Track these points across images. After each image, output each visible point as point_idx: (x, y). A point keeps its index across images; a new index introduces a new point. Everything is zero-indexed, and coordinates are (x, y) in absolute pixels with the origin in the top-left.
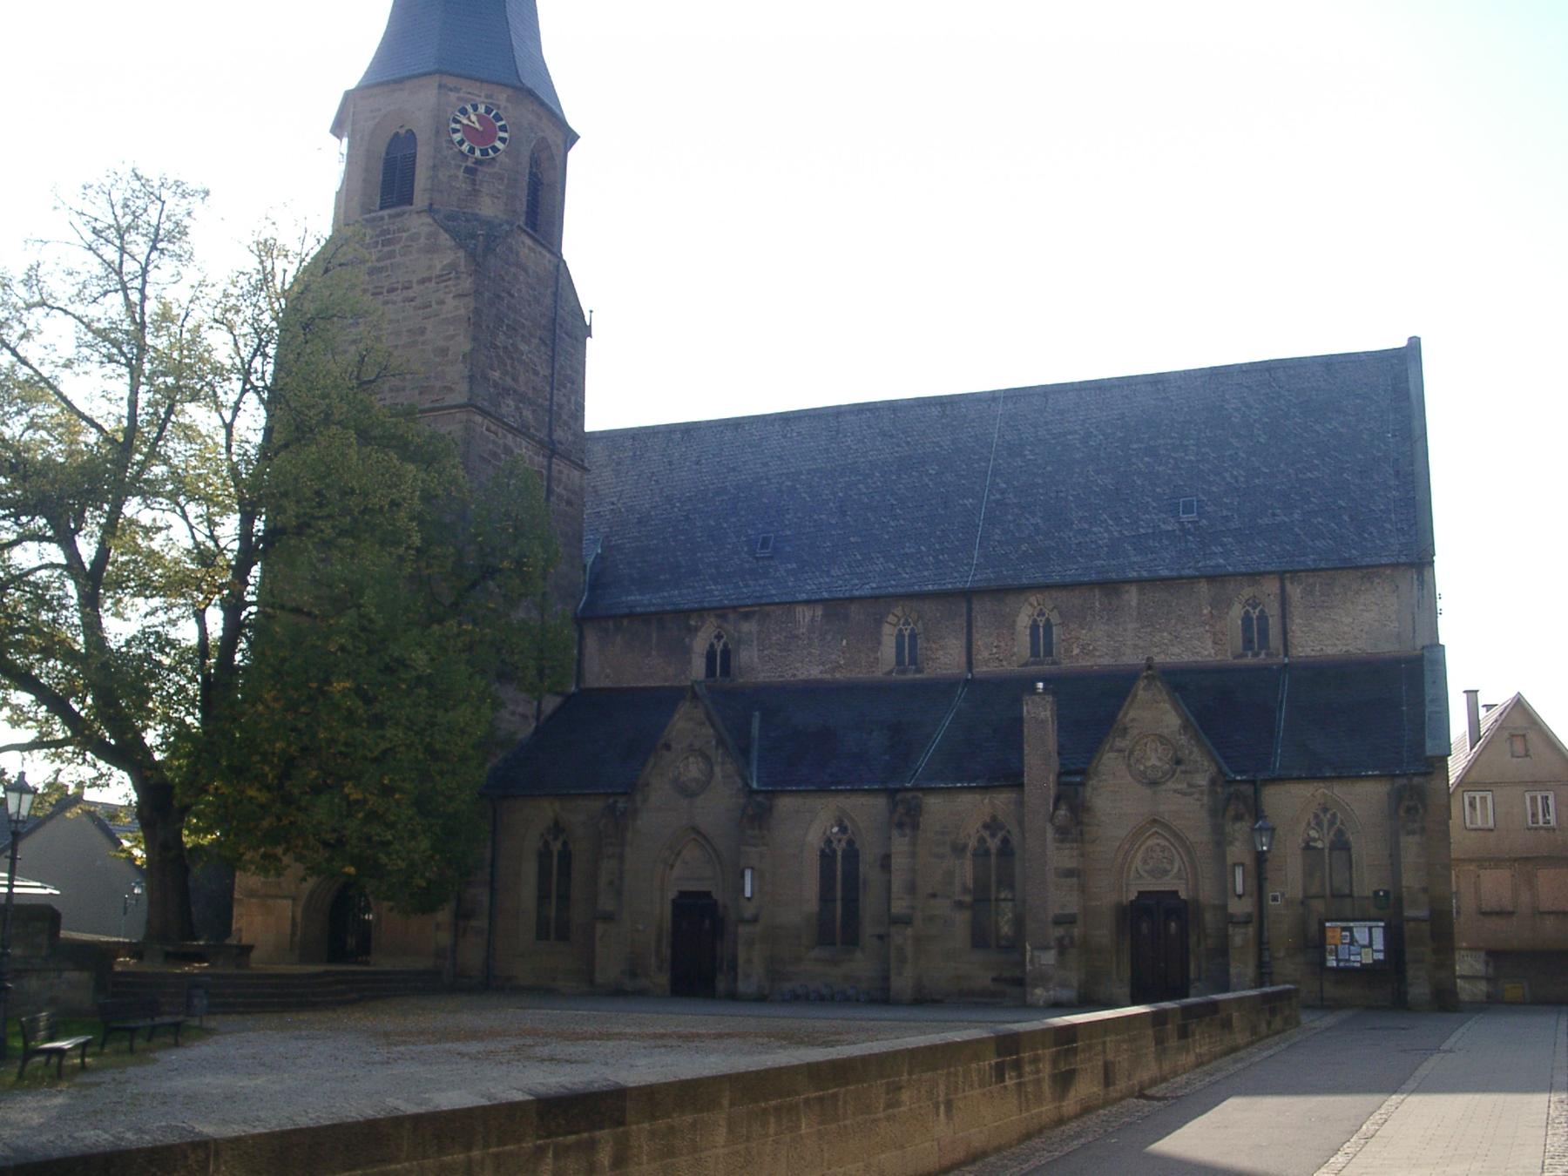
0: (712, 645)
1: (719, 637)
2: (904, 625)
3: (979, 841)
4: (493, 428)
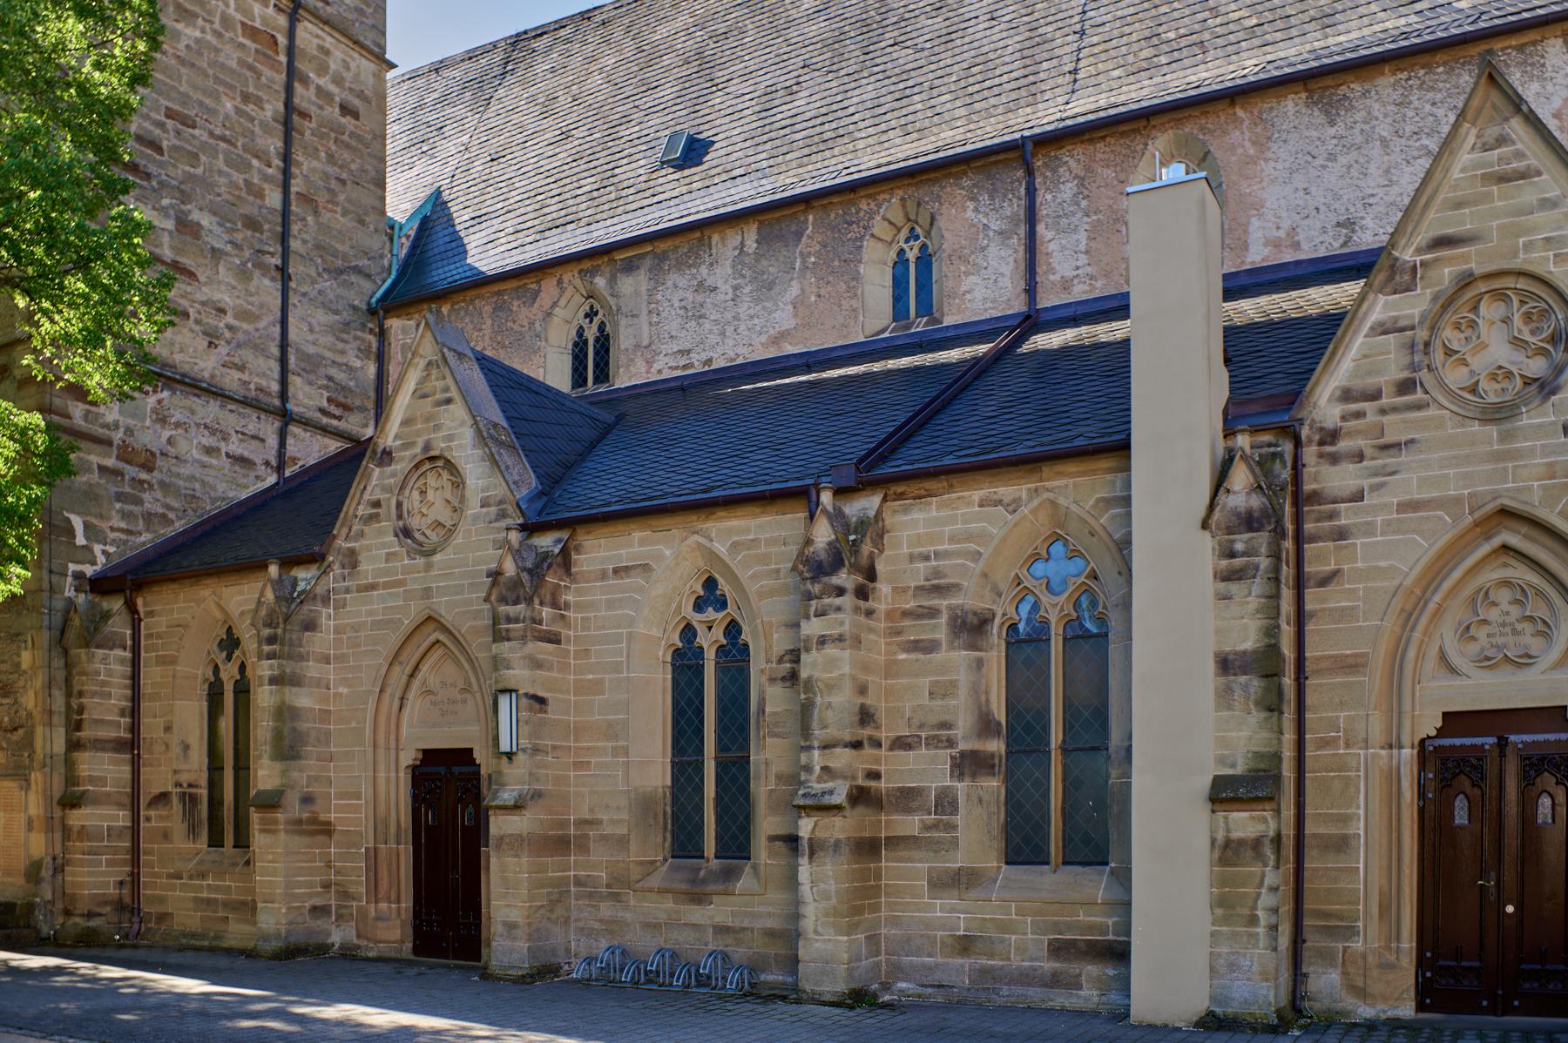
1: (591, 315)
2: (907, 241)
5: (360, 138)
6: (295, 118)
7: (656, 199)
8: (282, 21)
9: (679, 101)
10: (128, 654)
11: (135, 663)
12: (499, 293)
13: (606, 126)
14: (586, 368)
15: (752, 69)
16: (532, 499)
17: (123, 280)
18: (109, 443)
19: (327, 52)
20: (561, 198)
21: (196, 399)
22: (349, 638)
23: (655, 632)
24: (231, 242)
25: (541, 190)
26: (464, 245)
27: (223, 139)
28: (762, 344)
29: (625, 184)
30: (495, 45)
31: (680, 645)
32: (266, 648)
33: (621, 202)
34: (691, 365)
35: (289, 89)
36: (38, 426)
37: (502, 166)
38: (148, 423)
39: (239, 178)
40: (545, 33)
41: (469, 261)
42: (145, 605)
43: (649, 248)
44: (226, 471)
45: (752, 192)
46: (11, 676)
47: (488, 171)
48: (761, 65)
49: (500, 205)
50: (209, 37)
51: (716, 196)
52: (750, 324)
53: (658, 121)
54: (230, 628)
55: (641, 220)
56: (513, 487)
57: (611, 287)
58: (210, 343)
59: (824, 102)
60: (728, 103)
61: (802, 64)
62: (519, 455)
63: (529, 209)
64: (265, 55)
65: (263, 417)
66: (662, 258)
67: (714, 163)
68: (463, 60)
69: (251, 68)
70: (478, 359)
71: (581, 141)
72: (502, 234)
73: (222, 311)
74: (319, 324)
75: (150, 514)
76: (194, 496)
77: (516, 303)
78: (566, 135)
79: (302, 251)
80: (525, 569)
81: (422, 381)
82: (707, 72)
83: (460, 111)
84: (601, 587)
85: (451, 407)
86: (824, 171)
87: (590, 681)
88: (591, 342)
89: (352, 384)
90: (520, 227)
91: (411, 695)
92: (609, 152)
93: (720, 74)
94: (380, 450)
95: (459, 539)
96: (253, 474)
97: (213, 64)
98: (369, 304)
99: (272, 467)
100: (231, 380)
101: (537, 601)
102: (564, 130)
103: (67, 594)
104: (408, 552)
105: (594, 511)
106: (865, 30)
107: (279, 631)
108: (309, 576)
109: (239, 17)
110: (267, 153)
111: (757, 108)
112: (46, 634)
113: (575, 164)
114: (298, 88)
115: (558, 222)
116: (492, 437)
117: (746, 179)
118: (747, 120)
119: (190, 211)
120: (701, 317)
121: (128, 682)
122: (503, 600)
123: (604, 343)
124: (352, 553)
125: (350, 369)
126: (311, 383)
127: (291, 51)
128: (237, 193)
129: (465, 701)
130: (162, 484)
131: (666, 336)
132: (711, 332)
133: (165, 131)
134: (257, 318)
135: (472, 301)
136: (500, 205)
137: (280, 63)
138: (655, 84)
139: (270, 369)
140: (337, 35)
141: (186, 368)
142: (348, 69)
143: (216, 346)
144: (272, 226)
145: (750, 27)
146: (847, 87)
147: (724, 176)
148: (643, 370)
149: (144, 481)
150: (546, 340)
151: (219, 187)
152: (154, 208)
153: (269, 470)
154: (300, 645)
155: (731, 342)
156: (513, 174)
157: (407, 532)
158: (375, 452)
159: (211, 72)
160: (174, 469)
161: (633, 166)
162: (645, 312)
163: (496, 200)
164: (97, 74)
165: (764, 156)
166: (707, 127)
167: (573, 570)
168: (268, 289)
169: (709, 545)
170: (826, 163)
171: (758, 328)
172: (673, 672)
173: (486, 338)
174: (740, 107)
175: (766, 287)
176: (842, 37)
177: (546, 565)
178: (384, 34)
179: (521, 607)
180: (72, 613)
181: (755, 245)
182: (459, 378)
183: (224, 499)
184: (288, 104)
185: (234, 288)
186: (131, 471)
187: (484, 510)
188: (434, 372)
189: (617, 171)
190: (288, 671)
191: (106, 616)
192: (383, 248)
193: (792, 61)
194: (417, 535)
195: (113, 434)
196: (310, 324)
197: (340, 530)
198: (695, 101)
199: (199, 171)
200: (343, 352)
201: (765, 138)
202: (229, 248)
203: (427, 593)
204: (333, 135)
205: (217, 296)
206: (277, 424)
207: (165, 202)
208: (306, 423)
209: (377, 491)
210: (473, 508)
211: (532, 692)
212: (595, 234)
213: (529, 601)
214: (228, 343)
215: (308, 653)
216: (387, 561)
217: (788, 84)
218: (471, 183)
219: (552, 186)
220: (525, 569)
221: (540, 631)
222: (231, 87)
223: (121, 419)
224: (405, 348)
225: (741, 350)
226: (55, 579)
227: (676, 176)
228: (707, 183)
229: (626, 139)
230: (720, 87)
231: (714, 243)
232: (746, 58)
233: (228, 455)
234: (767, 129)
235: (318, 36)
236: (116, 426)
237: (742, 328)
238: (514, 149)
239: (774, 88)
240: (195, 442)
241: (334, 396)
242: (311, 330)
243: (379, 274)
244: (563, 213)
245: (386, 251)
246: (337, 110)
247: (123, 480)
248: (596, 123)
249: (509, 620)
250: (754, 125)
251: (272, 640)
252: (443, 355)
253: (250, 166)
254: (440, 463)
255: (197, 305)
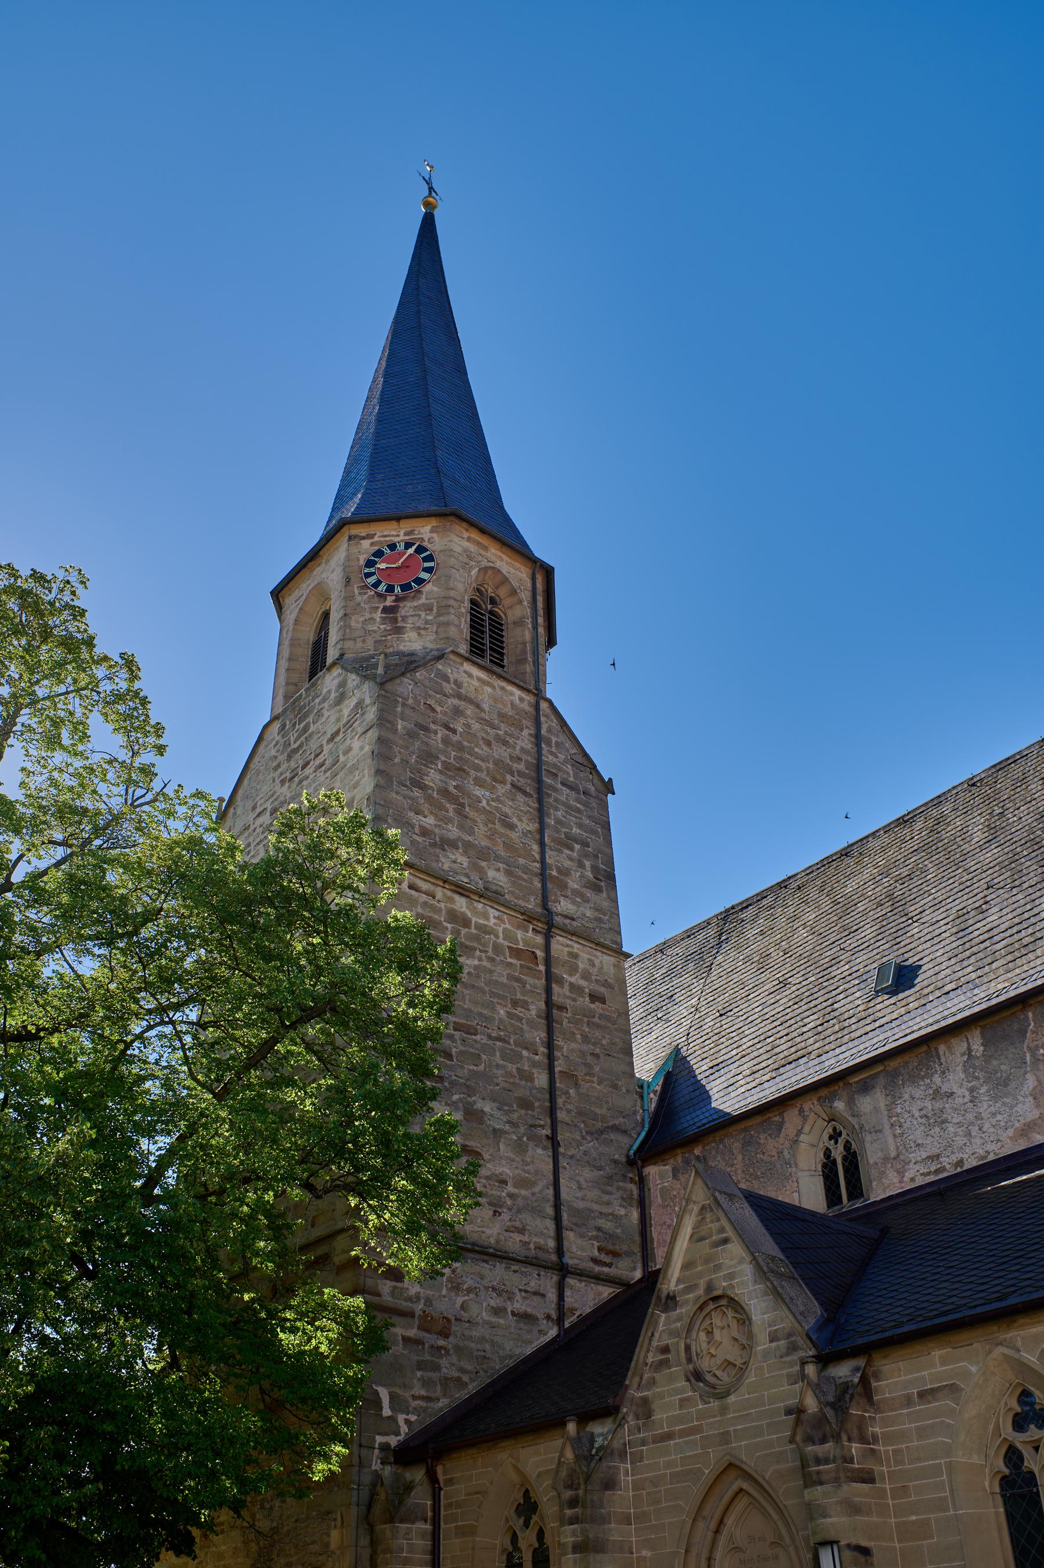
0: (827, 1153)
1: (835, 1136)
3: (1020, 1401)
4: (424, 886)
5: (607, 1018)
6: (555, 1012)
7: (877, 1024)
8: (540, 939)
9: (880, 937)
10: (428, 1527)
11: (435, 1536)
12: (746, 1130)
13: (818, 970)
14: (838, 1186)
15: (940, 899)
16: (821, 1326)
17: (441, 1176)
18: (412, 1315)
19: (576, 956)
20: (789, 1037)
21: (485, 1265)
22: (648, 1494)
23: (976, 1459)
24: (509, 1122)
25: (770, 1034)
26: (707, 1092)
27: (499, 1039)
28: (1010, 1138)
29: (846, 1016)
30: (708, 922)
31: (1007, 1471)
32: (568, 1512)
33: (846, 1031)
34: (943, 1169)
35: (548, 991)
36: (358, 1307)
37: (730, 1019)
38: (444, 1292)
39: (512, 1068)
40: (750, 905)
41: (713, 1105)
42: (445, 1473)
43: (881, 1068)
44: (512, 1330)
45: (968, 1002)
46: (320, 1558)
47: (718, 1025)
48: (948, 894)
49: (734, 1052)
50: (484, 963)
51: (934, 1012)
52: (994, 1121)
53: (865, 957)
54: (527, 1492)
55: (867, 1044)
56: (800, 1318)
57: (851, 1108)
58: (495, 1212)
59: (1015, 914)
60: (926, 931)
61: (985, 886)
62: (800, 1285)
63: (761, 1051)
64: (528, 968)
65: (542, 1273)
66: (895, 1074)
67: (926, 983)
68: (683, 939)
69: (518, 980)
70: (746, 1197)
71: (798, 986)
72: (740, 1077)
73: (504, 1182)
74: (586, 1180)
75: (446, 1379)
76: (485, 1357)
77: (762, 1136)
78: (784, 984)
79: (567, 1119)
80: (828, 1404)
81: (696, 1227)
82: (900, 909)
83: (686, 979)
84: (907, 1414)
85: (729, 1246)
86: (1031, 972)
87: (913, 1522)
88: (839, 1161)
89: (618, 1231)
90: (755, 1069)
91: (718, 1555)
92: (825, 991)
93: (913, 908)
94: (664, 1295)
95: (751, 1378)
96: (535, 1329)
97: (488, 983)
98: (628, 1156)
99: (553, 1320)
100: (513, 1243)
101: (844, 1437)
102: (781, 979)
103: (374, 1468)
104: (701, 1396)
105: (887, 1334)
106: (1036, 847)
107: (581, 1492)
108: (605, 1430)
109: (506, 943)
110: (534, 1044)
111: (954, 930)
112: (354, 1510)
113: (796, 1006)
114: (555, 987)
115: (790, 1059)
116: (772, 1271)
117: (959, 991)
118: (947, 942)
119: (475, 1102)
120: (943, 1122)
121: (428, 1557)
122: (809, 1440)
123: (852, 1160)
124: (645, 1402)
125: (616, 1218)
126: (582, 1236)
127: (548, 961)
128: (512, 1080)
129: (776, 1557)
130: (458, 1349)
131: (912, 1145)
132: (956, 1134)
133: (454, 1041)
134: (533, 1184)
135: (721, 1140)
136: (734, 1052)
137: (540, 971)
138: (855, 928)
139: (547, 1228)
140: (501, 909)
141: (475, 1237)
142: (594, 965)
143: (500, 1214)
144: (541, 1103)
145: (930, 865)
146: (1033, 897)
147: (938, 993)
148: (896, 1180)
149: (442, 1347)
150: (796, 1166)
151: (497, 1078)
152: (447, 1104)
153: (550, 1324)
154: (602, 1507)
155: (978, 1141)
156: (741, 1024)
157: (697, 1376)
158: (659, 1298)
159: (487, 989)
160: (467, 1333)
161: (850, 998)
162: (887, 1126)
163: (730, 1048)
164: (411, 1011)
165: (970, 969)
166: (911, 954)
167: (875, 1398)
168: (540, 1157)
169: (1017, 1356)
170: (1032, 964)
171: (1002, 1124)
172: (1005, 1504)
173: (739, 1172)
174: (937, 932)
175: (1001, 1085)
176: (1016, 857)
177: (848, 1396)
178: (620, 933)
179: (829, 1445)
180: (378, 1487)
181: (982, 1048)
182: (733, 1218)
183: (511, 1357)
184: (549, 1002)
185: (513, 1160)
186: (431, 1339)
187: (774, 1344)
188: (708, 1215)
189: (836, 1006)
190: (591, 1536)
191: (409, 1487)
192: (635, 1105)
193: (976, 885)
194: (709, 1378)
195: (414, 1306)
196: (578, 1182)
197: (632, 1380)
198: (895, 935)
199: (481, 1068)
200: (608, 1203)
201: (968, 953)
202: (507, 1127)
203: (725, 1438)
204: (585, 1019)
205: (499, 1170)
206: (555, 1278)
207: (455, 1097)
208: (581, 1274)
209: (665, 1336)
210: (763, 1344)
211: (854, 1541)
212: (827, 1064)
213: (837, 1438)
214: (510, 1209)
215: (609, 1514)
216: (681, 1407)
217: (977, 905)
218: (705, 1038)
219: (779, 1028)
220: (828, 1404)
221: (853, 1470)
222: (504, 998)
223: (422, 1291)
224: (664, 1191)
225: (990, 1147)
226: (364, 1451)
227: (892, 1000)
228: (923, 1001)
229: (838, 977)
230: (915, 919)
231: (941, 1053)
232: (933, 891)
233: (513, 1314)
234: (967, 945)
235: (568, 946)
236: (418, 1297)
237: (986, 1126)
238: (739, 1003)
239: (965, 911)
240: (484, 1305)
241: (603, 1245)
242: (580, 1188)
243: (634, 1129)
244: (793, 1050)
245: (638, 1108)
246: (587, 999)
247: (423, 1348)
248: (809, 969)
249: (818, 1461)
250: (954, 945)
251: (573, 1503)
252: (716, 1199)
253: (521, 1056)
254: (724, 1302)
255: (483, 1181)
